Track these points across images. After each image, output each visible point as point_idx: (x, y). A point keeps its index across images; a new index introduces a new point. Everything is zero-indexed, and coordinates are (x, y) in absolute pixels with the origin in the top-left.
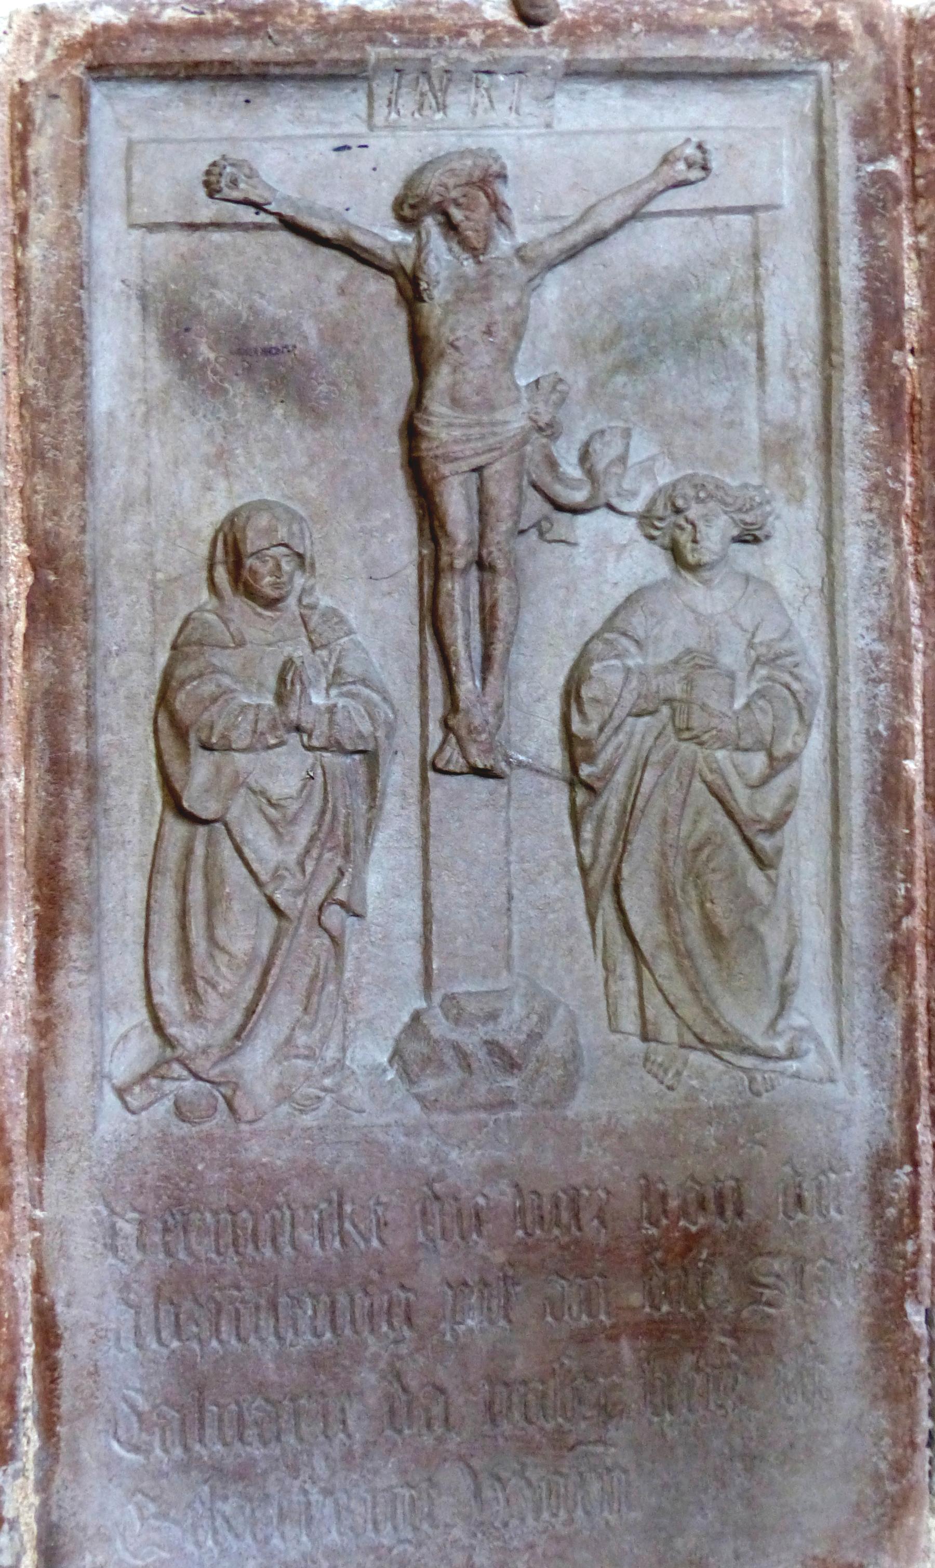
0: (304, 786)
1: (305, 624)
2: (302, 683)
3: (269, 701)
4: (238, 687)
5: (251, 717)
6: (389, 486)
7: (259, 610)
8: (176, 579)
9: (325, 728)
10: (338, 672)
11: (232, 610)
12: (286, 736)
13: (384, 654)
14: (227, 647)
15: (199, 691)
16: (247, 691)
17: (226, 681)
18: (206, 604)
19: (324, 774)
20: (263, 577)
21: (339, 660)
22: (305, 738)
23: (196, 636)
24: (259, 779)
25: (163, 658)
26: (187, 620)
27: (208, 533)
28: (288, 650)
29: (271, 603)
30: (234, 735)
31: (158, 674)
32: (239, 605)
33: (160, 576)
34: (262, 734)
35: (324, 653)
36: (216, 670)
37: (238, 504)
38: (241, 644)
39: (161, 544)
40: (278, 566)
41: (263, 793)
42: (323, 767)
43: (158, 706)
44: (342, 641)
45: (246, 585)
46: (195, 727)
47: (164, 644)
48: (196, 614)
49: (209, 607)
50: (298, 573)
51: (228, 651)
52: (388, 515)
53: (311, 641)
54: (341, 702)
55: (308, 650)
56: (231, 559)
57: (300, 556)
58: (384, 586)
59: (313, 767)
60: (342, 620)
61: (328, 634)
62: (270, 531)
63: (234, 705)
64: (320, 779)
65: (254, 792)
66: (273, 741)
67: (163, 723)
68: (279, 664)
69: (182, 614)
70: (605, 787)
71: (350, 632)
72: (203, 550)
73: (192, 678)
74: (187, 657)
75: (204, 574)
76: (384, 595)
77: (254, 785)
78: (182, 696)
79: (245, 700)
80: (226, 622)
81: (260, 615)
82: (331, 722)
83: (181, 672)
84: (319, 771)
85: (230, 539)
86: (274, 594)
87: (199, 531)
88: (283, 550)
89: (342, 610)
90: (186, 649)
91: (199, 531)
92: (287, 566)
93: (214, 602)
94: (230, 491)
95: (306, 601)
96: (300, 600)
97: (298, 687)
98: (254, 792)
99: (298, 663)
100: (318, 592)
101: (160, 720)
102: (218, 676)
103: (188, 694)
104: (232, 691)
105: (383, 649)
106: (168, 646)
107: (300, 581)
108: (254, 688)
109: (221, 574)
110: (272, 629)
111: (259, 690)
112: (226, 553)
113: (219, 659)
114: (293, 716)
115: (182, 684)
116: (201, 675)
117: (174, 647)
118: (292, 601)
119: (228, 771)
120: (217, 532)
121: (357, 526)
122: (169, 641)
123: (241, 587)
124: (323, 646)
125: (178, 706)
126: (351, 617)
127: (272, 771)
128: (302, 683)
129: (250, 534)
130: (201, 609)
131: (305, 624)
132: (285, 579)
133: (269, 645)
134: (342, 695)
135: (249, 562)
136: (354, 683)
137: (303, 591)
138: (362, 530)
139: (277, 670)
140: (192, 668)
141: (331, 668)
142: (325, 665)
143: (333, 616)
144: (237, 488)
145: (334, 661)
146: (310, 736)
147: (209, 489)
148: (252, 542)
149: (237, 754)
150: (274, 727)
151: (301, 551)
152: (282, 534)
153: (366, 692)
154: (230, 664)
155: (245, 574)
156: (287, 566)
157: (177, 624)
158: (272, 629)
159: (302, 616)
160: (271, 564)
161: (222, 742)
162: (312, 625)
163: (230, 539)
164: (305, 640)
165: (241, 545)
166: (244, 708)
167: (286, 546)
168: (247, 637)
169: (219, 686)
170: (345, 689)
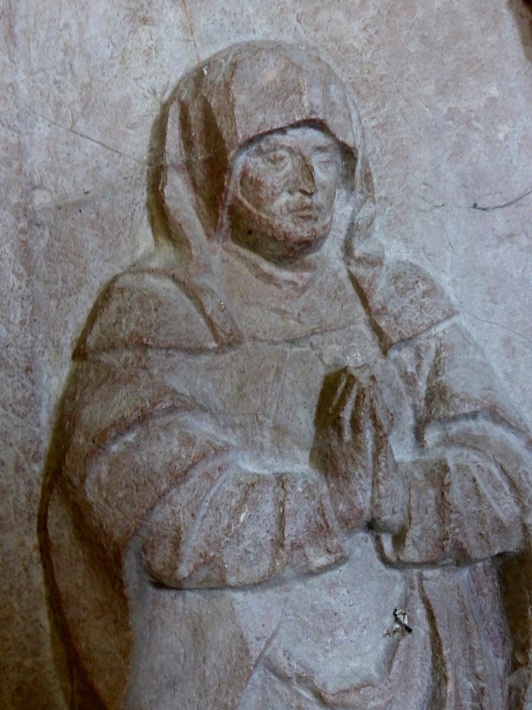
0: (392, 651)
1: (364, 298)
2: (377, 425)
3: (300, 465)
4: (231, 438)
5: (268, 509)
6: (492, 39)
7: (267, 267)
8: (79, 206)
9: (430, 519)
10: (437, 394)
11: (207, 268)
12: (347, 544)
13: (512, 353)
14: (203, 350)
15: (141, 458)
16: (249, 443)
17: (204, 428)
18: (150, 256)
19: (431, 617)
20: (275, 195)
21: (436, 370)
22: (387, 543)
23: (128, 328)
24: (296, 651)
25: (54, 379)
26: (106, 294)
27: (146, 109)
28: (332, 351)
29: (294, 252)
30: (230, 558)
31: (45, 416)
32: (219, 259)
33: (41, 198)
34: (297, 546)
35: (406, 355)
36: (180, 405)
37: (205, 56)
38: (229, 341)
39: (42, 129)
40: (308, 171)
41: (305, 680)
42: (426, 602)
43: (48, 489)
44: (440, 328)
45: (235, 212)
46: (135, 545)
47: (58, 347)
48: (128, 280)
49: (154, 264)
50: (342, 193)
51: (205, 359)
52: (494, 91)
53: (377, 330)
54: (451, 457)
55: (374, 351)
56: (200, 155)
57: (348, 153)
58: (499, 221)
59: (406, 601)
60: (433, 290)
61: (412, 317)
62: (287, 91)
63: (226, 484)
64: (422, 629)
65: (284, 678)
66: (321, 560)
67: (62, 532)
68: (317, 385)
69: (96, 284)
70: (234, 323)
71: (450, 314)
72: (137, 144)
73: (123, 426)
74: (111, 377)
75: (142, 195)
76: (501, 239)
77: (282, 661)
78: (101, 469)
79: (250, 466)
80: (194, 294)
81: (269, 278)
82: (443, 505)
83: (96, 413)
84: (420, 611)
85: (195, 114)
86: (302, 231)
87: (126, 105)
88: (313, 136)
89: (429, 269)
90: (105, 358)
91: (126, 105)
92: (325, 174)
93: (168, 251)
94: (189, 29)
95: (360, 249)
96: (348, 249)
97: (368, 435)
98: (284, 678)
99: (363, 379)
100: (379, 234)
101: (51, 522)
102: (186, 418)
103: (115, 463)
104: (220, 451)
105: (507, 341)
106: (68, 352)
107: (343, 210)
108: (266, 438)
109: (179, 193)
110: (296, 307)
111: (277, 442)
112: (188, 143)
113: (184, 377)
114: (363, 501)
115: (101, 441)
116: (144, 418)
117: (80, 353)
118: (331, 249)
119: (220, 635)
120: (165, 107)
121: (443, 108)
122: (68, 340)
123: (225, 219)
124: (405, 341)
125: (92, 493)
126: (445, 280)
127: (323, 625)
128: (377, 425)
129: (241, 98)
130: (137, 269)
131: (364, 298)
132: (319, 198)
133: (293, 342)
134: (447, 441)
135: (241, 161)
136: (474, 415)
137: (352, 228)
138: (452, 114)
139: (314, 399)
140: (122, 402)
141: (422, 386)
142: (410, 380)
143: (409, 277)
144: (202, 22)
145: (426, 370)
146: (399, 540)
147: (144, 21)
148: (248, 114)
149: (239, 596)
150: (321, 531)
151: (350, 142)
152: (312, 101)
153: (498, 432)
154: (209, 388)
155: (233, 187)
156: (325, 174)
157: (85, 303)
158: (296, 307)
159: (354, 280)
160: (289, 165)
161: (203, 573)
162: (376, 300)
163: (195, 114)
164: (365, 329)
165: (222, 123)
166: (251, 486)
167: (319, 125)
168: (241, 325)
169: (188, 441)
170: (455, 429)
